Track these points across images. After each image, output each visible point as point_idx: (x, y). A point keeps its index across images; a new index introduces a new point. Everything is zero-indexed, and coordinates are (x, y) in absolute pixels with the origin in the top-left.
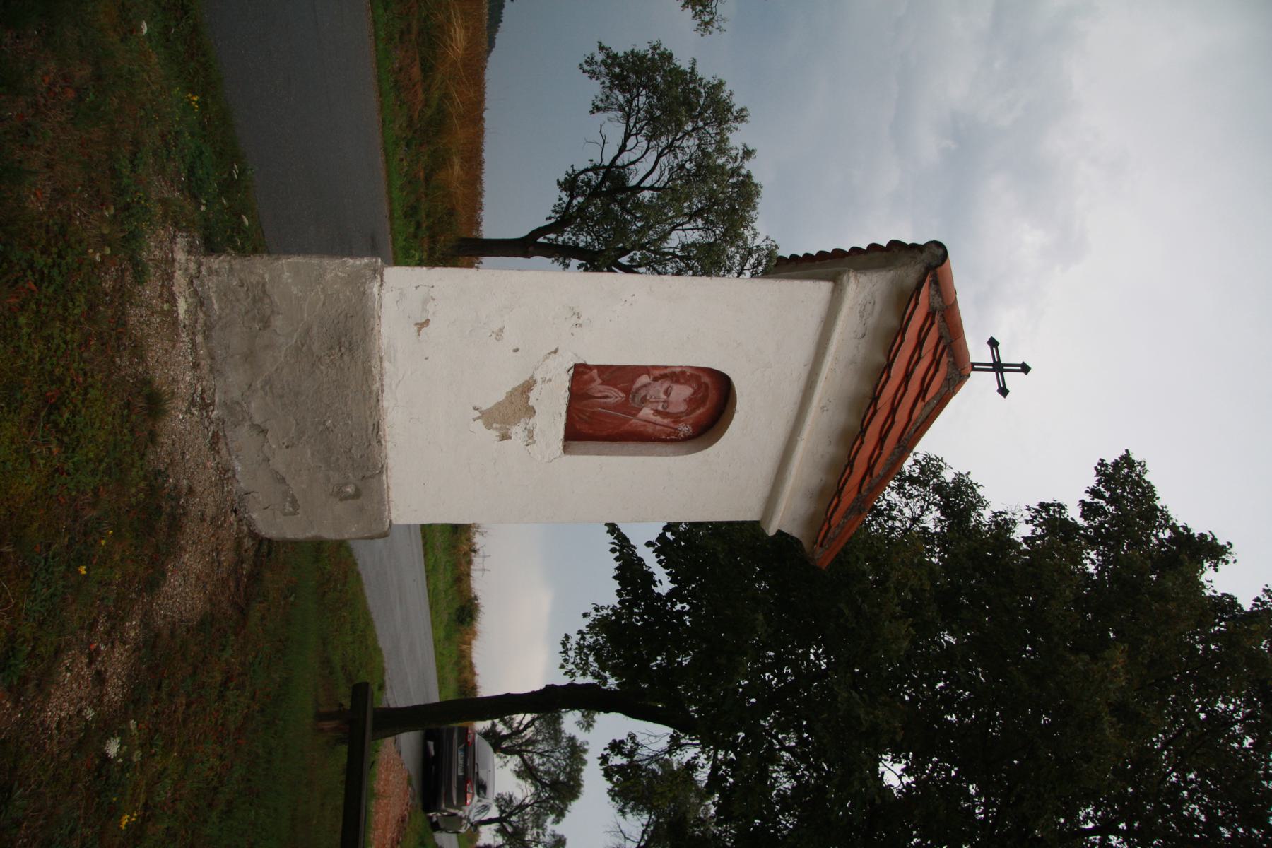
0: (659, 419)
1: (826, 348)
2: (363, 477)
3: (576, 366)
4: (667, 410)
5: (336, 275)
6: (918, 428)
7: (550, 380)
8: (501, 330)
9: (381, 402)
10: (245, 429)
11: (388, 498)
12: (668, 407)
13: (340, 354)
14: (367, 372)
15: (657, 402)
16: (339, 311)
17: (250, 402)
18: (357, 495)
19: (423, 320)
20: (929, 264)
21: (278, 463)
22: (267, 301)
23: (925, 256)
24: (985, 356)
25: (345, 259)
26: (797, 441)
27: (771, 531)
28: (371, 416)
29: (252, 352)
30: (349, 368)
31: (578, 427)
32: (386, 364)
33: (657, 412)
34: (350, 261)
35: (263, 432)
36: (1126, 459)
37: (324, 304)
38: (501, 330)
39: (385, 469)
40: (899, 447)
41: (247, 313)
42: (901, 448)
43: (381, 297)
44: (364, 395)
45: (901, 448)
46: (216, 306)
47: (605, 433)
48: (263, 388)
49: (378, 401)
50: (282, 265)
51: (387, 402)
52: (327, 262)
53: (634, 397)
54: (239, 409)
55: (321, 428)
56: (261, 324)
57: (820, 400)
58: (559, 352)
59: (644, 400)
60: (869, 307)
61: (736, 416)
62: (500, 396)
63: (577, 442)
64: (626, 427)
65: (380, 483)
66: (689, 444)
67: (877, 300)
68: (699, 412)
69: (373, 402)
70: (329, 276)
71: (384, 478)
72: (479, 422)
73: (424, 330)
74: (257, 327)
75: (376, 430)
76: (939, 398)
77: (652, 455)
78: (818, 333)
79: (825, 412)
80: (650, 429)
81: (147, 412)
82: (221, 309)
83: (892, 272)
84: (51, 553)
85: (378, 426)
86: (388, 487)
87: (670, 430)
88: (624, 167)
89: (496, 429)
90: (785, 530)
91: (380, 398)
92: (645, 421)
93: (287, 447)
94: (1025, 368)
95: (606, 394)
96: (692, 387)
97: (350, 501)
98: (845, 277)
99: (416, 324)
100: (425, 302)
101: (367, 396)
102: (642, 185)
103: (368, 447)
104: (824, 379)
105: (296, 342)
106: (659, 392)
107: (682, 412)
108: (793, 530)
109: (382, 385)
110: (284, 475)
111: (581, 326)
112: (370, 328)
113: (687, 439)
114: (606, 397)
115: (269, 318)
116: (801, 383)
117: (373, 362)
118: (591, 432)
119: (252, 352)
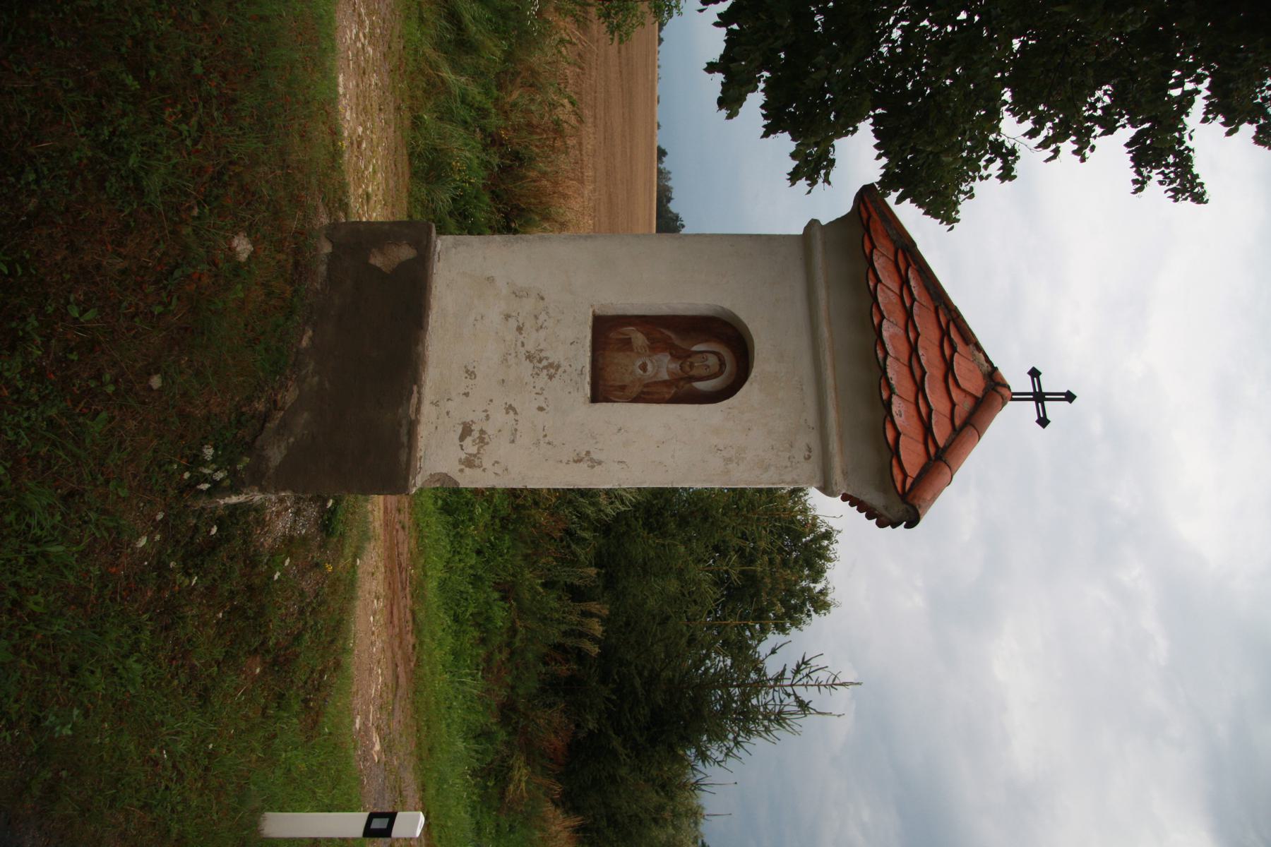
24: (1025, 385)
36: (1049, 422)
81: (676, 682)
84: (23, 433)
88: (998, 392)
94: (1070, 397)
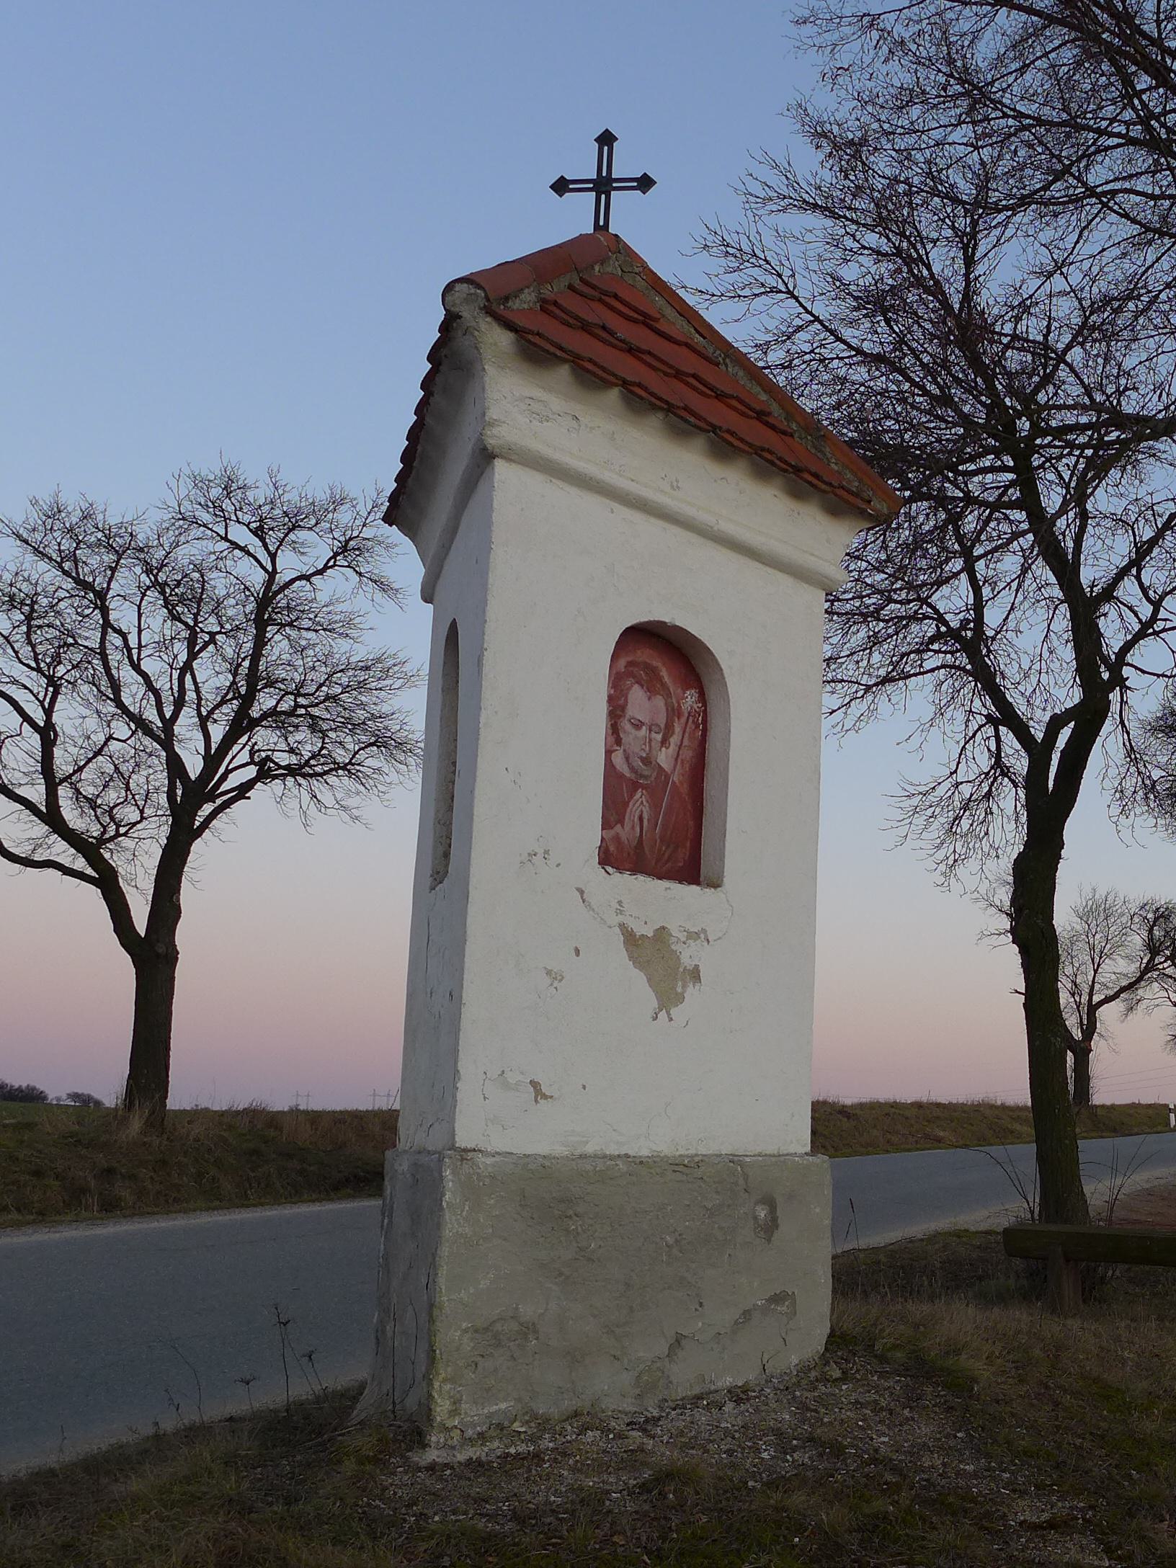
0: (674, 740)
4: (663, 726)
7: (620, 903)
8: (549, 973)
12: (657, 725)
13: (575, 1218)
22: (498, 1327)
25: (444, 1204)
32: (590, 1149)
33: (664, 742)
35: (678, 1341)
38: (549, 973)
39: (736, 1158)
42: (727, 360)
45: (727, 360)
46: (503, 1406)
47: (691, 823)
52: (447, 1233)
53: (642, 776)
55: (675, 1251)
59: (646, 761)
62: (638, 978)
64: (684, 789)
68: (664, 673)
71: (748, 1159)
75: (681, 1168)
80: (687, 754)
92: (676, 760)
93: (701, 1305)
97: (779, 1213)
99: (536, 1101)
107: (666, 704)
111: (546, 852)
113: (702, 697)
115: (521, 1324)
118: (688, 844)
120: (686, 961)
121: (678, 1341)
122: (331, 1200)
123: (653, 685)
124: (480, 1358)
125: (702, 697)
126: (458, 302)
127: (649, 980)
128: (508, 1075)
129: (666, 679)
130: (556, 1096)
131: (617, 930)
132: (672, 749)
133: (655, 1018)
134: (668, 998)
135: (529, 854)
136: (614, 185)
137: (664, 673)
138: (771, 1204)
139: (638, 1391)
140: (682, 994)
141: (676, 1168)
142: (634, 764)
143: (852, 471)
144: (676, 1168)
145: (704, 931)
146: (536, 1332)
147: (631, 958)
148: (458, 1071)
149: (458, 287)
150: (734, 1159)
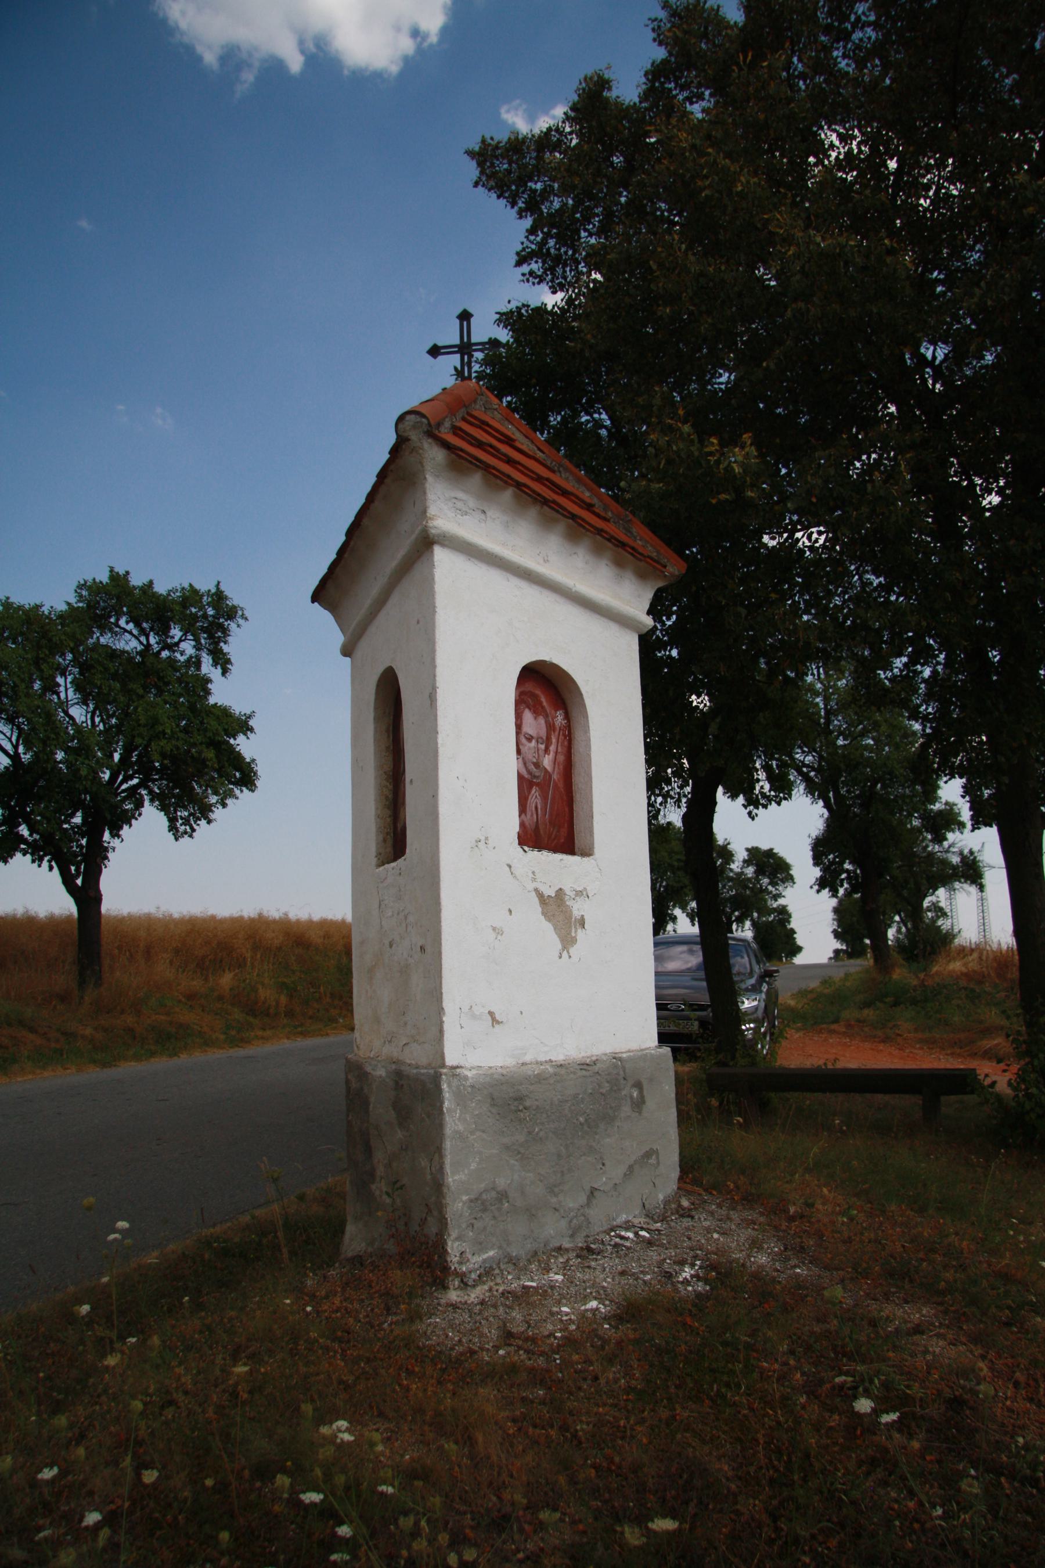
0: (552, 748)
1: (496, 556)
2: (625, 1079)
3: (521, 843)
4: (545, 738)
5: (459, 1119)
6: (539, 449)
7: (533, 873)
8: (494, 929)
9: (563, 1063)
10: (592, 1213)
11: (638, 1051)
12: (542, 738)
13: (524, 1111)
14: (540, 1079)
15: (538, 750)
16: (489, 1114)
17: (569, 1209)
18: (638, 1085)
19: (490, 1018)
20: (425, 433)
21: (617, 1172)
22: (484, 1196)
23: (414, 436)
25: (445, 1110)
26: (576, 591)
27: (649, 621)
28: (574, 1073)
29: (527, 1210)
30: (536, 1100)
31: (562, 840)
32: (528, 1058)
33: (547, 750)
34: (446, 1104)
35: (593, 1191)
37: (484, 1132)
38: (494, 929)
39: (617, 1056)
40: (560, 472)
41: (494, 1217)
42: (561, 469)
43: (473, 1068)
44: (558, 1082)
45: (561, 469)
46: (491, 1253)
47: (567, 809)
48: (556, 1195)
49: (561, 1065)
50: (454, 1181)
51: (559, 1057)
52: (448, 1131)
53: (535, 777)
54: (575, 1221)
55: (586, 1128)
56: (504, 1201)
57: (538, 563)
58: (509, 862)
59: (537, 765)
60: (459, 504)
61: (555, 661)
62: (548, 927)
63: (576, 841)
64: (561, 785)
65: (630, 1059)
66: (574, 713)
67: (453, 494)
68: (543, 699)
69: (563, 1071)
70: (461, 1128)
71: (624, 1055)
72: (572, 950)
73: (498, 1017)
74: (506, 1204)
75: (585, 1067)
76: (506, 422)
77: (589, 756)
78: (476, 562)
79: (549, 558)
80: (561, 758)
82: (492, 1248)
83: (427, 476)
85: (583, 1064)
86: (629, 1051)
87: (561, 737)
89: (576, 932)
90: (647, 607)
91: (559, 1063)
92: (555, 764)
93: (603, 1164)
95: (534, 809)
96: (524, 709)
97: (645, 1093)
98: (433, 531)
99: (493, 1026)
100: (474, 1017)
101: (559, 1078)
102: (12, 753)
103: (600, 1075)
104: (522, 559)
105: (517, 1160)
106: (529, 749)
107: (546, 722)
108: (648, 596)
109: (546, 1062)
110: (627, 1166)
111: (487, 839)
112: (502, 1078)
113: (567, 717)
114: (536, 808)
115: (498, 1193)
116: (524, 585)
117: (530, 1073)
118: (566, 825)
119: (527, 1210)
120: (576, 913)
121: (593, 1191)
122: (304, 1034)
123: (537, 710)
124: (474, 1221)
125: (567, 717)
126: (408, 428)
127: (555, 929)
128: (474, 1008)
129: (545, 704)
130: (505, 1021)
131: (534, 893)
132: (552, 754)
133: (560, 957)
134: (567, 941)
135: (476, 841)
136: (474, 348)
137: (543, 699)
138: (638, 1085)
139: (570, 1232)
140: (575, 937)
141: (582, 1067)
142: (530, 768)
143: (652, 545)
144: (582, 1067)
145: (585, 889)
146: (507, 1197)
147: (543, 913)
148: (443, 1009)
149: (408, 417)
150: (616, 1057)
